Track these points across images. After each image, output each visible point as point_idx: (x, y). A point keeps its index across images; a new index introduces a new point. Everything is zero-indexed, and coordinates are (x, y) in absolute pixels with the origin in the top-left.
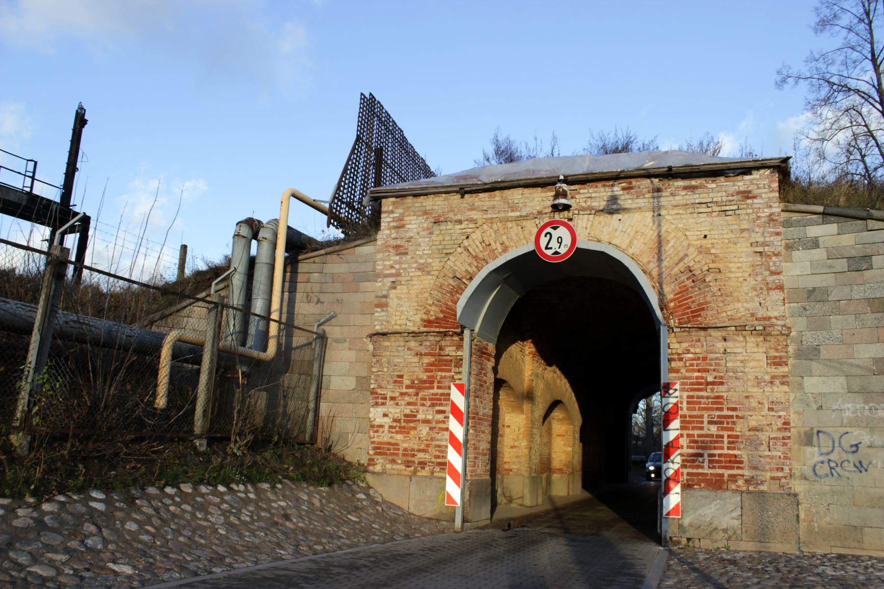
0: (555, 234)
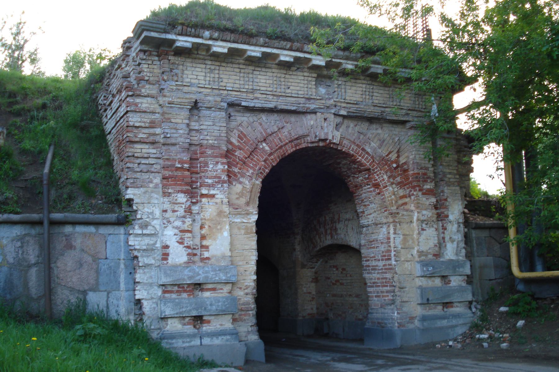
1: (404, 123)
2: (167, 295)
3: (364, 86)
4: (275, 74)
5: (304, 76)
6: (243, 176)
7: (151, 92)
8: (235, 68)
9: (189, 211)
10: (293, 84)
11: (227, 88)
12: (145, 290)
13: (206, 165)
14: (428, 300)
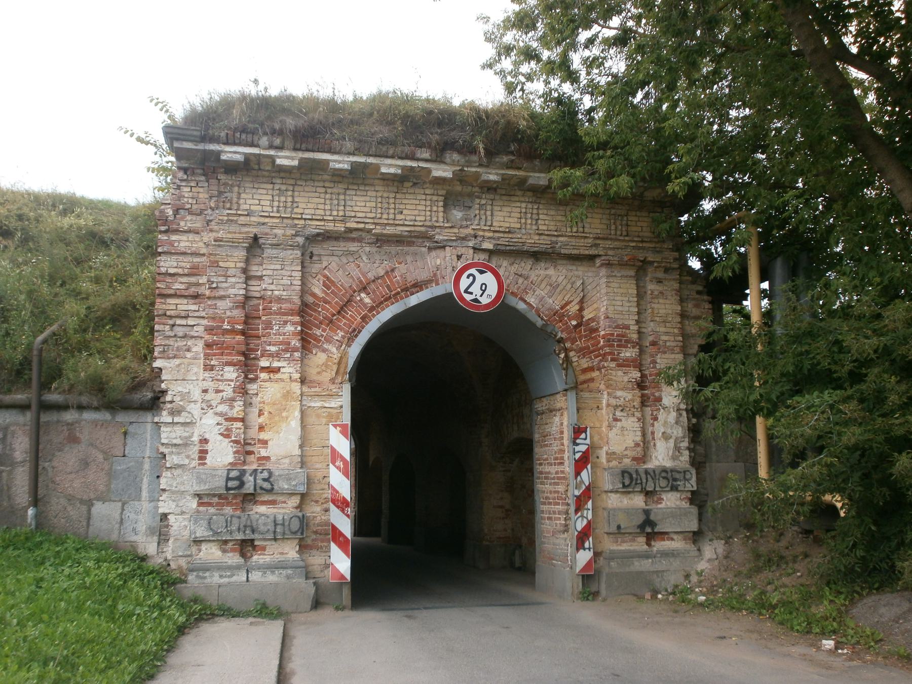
0: (481, 279)
1: (592, 258)
2: (201, 509)
3: (524, 205)
4: (379, 194)
5: (427, 194)
6: (329, 340)
7: (194, 225)
9: (243, 391)
10: (408, 207)
11: (304, 216)
12: (174, 501)
13: (269, 325)
14: (619, 527)
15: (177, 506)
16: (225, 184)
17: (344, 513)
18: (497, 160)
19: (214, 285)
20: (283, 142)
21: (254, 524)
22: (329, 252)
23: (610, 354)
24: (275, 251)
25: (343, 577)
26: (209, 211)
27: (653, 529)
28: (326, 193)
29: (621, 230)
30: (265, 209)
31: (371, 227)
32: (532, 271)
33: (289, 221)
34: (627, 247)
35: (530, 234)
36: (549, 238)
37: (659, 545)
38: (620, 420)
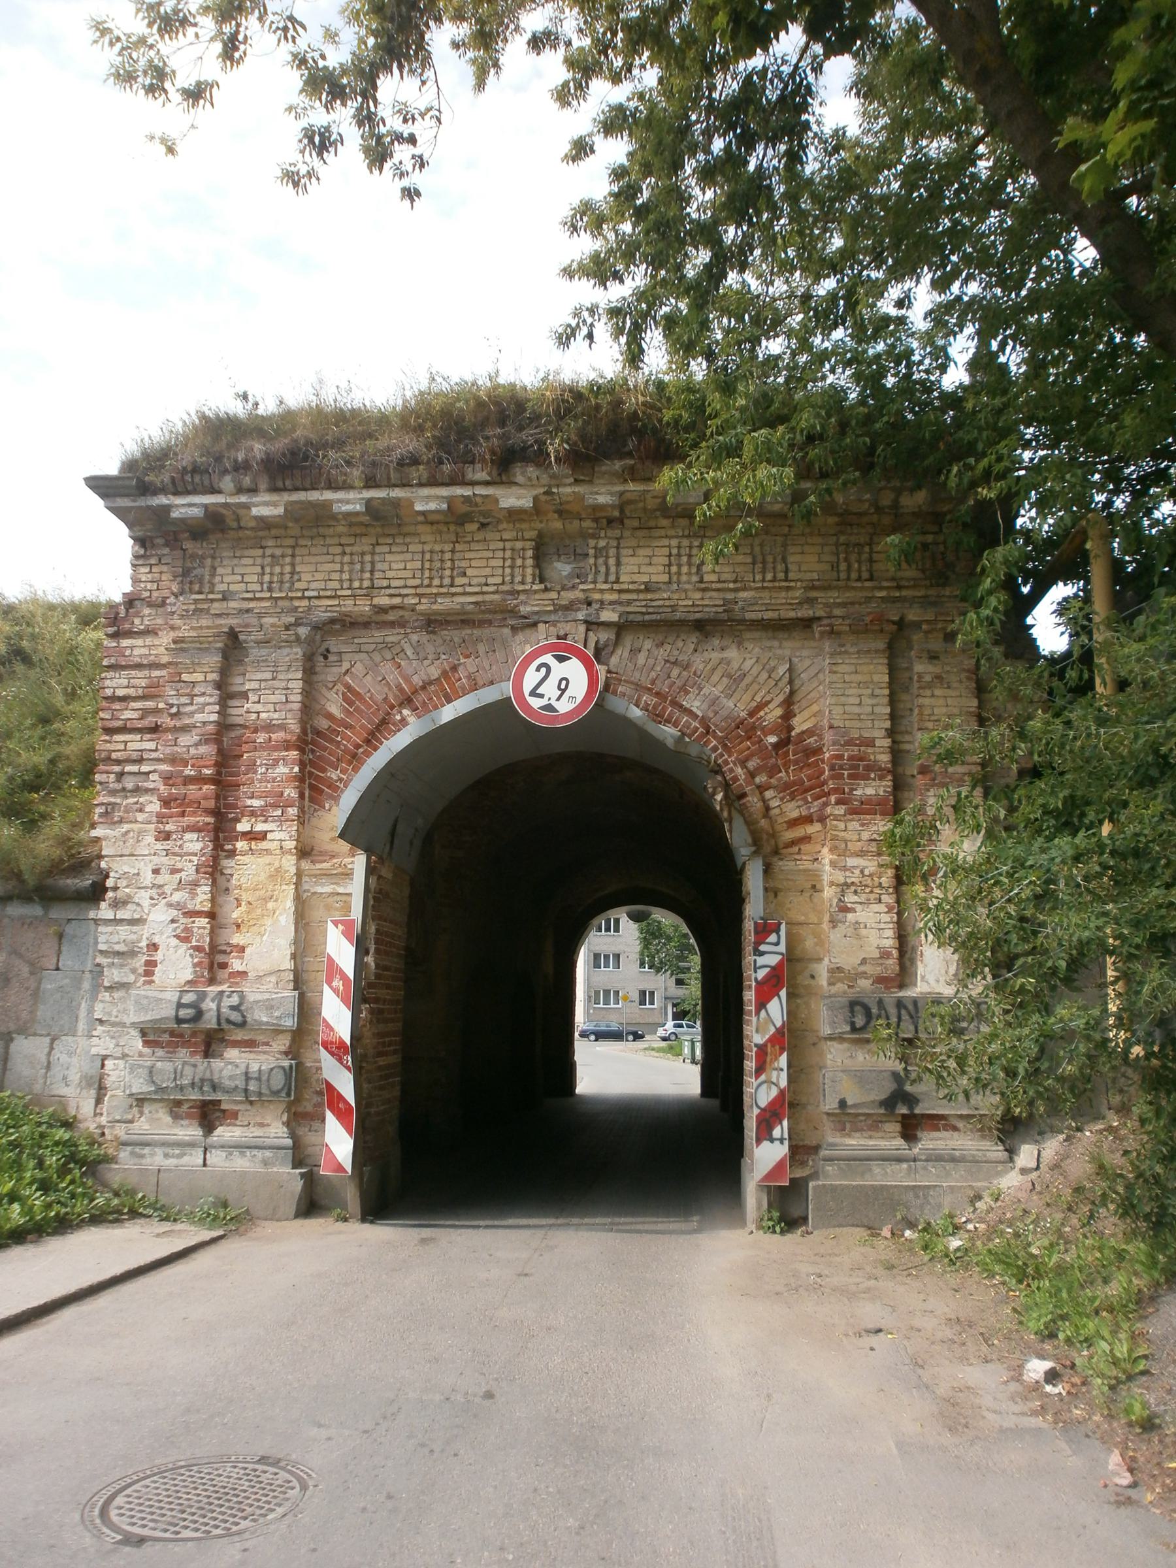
0: (559, 670)
1: (807, 624)
3: (674, 542)
4: (427, 548)
8: (330, 545)
10: (474, 563)
11: (307, 594)
12: (113, 1038)
15: (117, 1045)
16: (193, 556)
17: (342, 1063)
18: (604, 468)
19: (174, 710)
20: (254, 481)
21: (216, 1077)
22: (353, 648)
23: (836, 791)
24: (264, 652)
25: (340, 1168)
26: (172, 599)
27: (911, 1108)
28: (344, 553)
29: (859, 571)
30: (251, 587)
31: (413, 601)
32: (696, 655)
33: (286, 603)
34: (869, 599)
35: (686, 591)
36: (721, 595)
37: (930, 1141)
38: (853, 910)
